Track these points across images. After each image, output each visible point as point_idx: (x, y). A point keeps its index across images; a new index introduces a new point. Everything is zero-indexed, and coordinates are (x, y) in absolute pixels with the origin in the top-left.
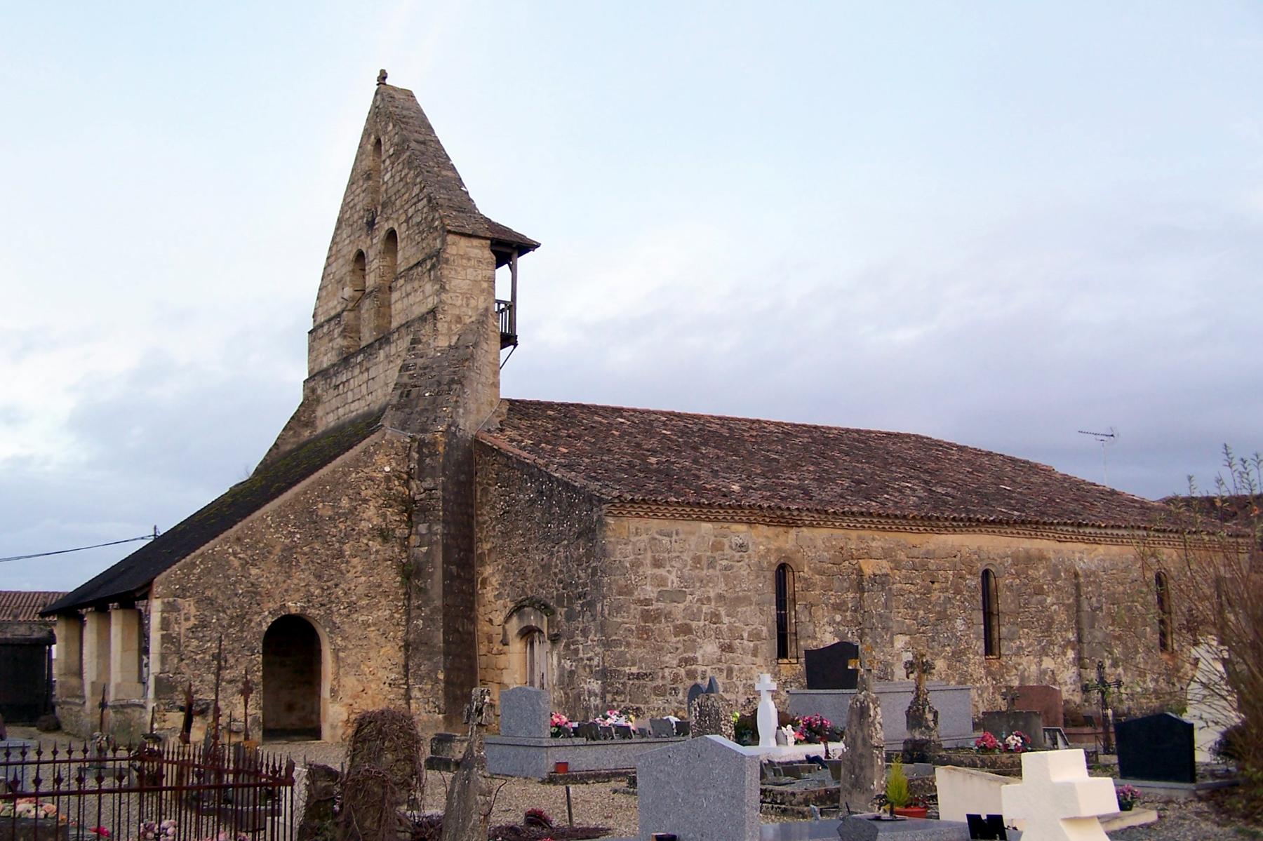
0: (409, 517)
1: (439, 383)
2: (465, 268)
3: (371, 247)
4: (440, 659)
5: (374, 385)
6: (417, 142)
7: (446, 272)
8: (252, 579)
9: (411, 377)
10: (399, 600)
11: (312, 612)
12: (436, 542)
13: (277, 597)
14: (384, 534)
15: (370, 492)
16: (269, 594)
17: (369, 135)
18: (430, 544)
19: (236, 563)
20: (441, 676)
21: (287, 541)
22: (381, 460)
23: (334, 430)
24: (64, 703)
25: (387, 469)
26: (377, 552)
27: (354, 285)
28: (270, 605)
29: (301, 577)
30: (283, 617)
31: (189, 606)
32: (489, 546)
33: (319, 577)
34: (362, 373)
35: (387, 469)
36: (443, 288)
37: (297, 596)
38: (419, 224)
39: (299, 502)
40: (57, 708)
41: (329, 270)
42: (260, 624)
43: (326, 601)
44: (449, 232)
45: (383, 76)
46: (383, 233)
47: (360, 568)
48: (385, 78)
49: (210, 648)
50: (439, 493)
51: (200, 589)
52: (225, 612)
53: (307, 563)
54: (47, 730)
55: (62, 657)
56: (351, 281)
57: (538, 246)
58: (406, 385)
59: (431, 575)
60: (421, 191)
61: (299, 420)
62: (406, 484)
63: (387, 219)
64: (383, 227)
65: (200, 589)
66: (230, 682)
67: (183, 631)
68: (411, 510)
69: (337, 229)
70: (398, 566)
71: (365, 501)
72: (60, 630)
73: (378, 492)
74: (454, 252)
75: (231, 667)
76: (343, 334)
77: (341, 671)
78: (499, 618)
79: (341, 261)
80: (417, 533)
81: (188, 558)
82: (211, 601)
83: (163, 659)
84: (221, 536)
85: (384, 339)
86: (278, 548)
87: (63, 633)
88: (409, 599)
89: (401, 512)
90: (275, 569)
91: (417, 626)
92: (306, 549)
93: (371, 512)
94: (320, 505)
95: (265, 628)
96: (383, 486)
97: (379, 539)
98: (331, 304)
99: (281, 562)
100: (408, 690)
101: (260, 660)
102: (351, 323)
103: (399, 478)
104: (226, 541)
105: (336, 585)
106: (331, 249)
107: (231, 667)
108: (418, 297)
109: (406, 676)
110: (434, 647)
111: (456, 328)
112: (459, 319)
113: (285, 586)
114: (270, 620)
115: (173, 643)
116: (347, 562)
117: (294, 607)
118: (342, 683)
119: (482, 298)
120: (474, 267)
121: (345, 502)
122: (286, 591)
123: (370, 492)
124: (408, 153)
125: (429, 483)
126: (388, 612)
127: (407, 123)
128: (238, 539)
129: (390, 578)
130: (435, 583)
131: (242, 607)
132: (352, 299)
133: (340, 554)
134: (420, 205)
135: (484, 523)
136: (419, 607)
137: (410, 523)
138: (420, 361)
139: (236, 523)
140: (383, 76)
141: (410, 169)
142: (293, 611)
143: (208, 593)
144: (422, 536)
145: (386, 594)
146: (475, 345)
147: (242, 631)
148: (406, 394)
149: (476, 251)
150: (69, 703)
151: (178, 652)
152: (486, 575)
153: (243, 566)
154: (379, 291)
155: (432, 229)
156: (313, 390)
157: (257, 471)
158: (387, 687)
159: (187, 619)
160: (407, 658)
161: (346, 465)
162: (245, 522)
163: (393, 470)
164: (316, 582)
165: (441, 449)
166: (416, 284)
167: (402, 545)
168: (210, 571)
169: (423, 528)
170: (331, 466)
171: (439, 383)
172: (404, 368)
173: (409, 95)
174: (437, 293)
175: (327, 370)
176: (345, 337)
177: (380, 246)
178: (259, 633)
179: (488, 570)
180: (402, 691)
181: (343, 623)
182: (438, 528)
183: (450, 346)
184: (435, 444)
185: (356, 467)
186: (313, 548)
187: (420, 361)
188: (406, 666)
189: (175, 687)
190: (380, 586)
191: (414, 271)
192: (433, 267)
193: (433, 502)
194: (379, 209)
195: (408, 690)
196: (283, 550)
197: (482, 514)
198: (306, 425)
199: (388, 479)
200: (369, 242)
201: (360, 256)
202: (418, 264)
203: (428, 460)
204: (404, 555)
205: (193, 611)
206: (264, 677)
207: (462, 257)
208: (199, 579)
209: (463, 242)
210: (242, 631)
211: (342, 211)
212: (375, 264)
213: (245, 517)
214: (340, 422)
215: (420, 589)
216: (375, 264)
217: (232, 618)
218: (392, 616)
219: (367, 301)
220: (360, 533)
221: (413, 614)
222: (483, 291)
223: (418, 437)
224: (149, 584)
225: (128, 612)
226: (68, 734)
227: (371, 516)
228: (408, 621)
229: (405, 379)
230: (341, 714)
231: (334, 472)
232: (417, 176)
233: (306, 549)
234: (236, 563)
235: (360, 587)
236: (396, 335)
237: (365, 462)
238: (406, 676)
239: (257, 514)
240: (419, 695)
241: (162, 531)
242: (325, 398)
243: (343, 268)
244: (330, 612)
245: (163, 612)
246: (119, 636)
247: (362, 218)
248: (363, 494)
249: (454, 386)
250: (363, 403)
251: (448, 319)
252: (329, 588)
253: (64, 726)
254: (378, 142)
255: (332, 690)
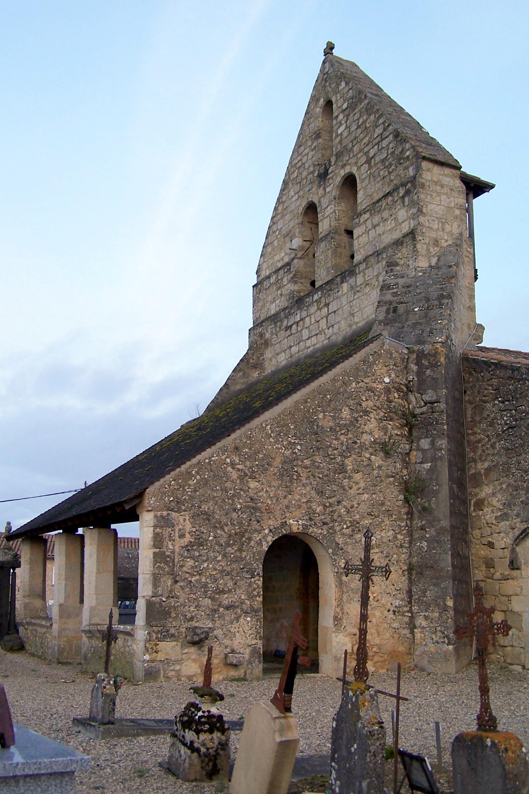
0: (410, 432)
1: (428, 300)
2: (439, 194)
3: (323, 196)
4: (448, 584)
5: (357, 306)
6: (370, 93)
7: (422, 196)
8: (251, 493)
9: (395, 294)
10: (401, 520)
11: (314, 531)
12: (441, 458)
13: (278, 513)
14: (386, 449)
15: (370, 403)
16: (269, 511)
17: (318, 100)
18: (434, 459)
19: (234, 475)
20: (450, 603)
21: (288, 453)
22: (381, 371)
23: (287, 368)
24: (29, 624)
25: (387, 380)
26: (380, 467)
27: (303, 236)
28: (271, 522)
29: (303, 492)
30: (285, 537)
31: (184, 521)
32: (486, 465)
33: (321, 493)
34: (319, 309)
35: (387, 380)
36: (420, 211)
37: (298, 513)
38: (383, 161)
39: (299, 410)
40: (21, 629)
41: (274, 228)
42: (260, 543)
43: (328, 520)
44: (424, 158)
45: (330, 47)
46: (338, 180)
47: (362, 485)
48: (332, 48)
49: (207, 568)
50: (443, 406)
51: (196, 502)
52: (222, 529)
53: (308, 478)
54: (11, 650)
55: (27, 579)
56: (300, 232)
57: (492, 187)
58: (391, 303)
59: (436, 493)
60: (385, 130)
61: (248, 362)
62: (405, 397)
63: (343, 166)
64: (338, 175)
65: (196, 502)
66: (227, 608)
67: (177, 549)
68: (412, 423)
69: (282, 190)
70: (400, 483)
71: (366, 413)
72: (25, 552)
73: (378, 404)
74: (429, 178)
75: (230, 591)
76: (294, 280)
77: (345, 598)
78: (503, 540)
79: (288, 217)
80: (418, 449)
81: (183, 468)
82: (208, 516)
83: (156, 580)
84: (219, 445)
85: (347, 272)
86: (279, 459)
87: (28, 556)
88: (411, 519)
89: (402, 426)
90: (276, 483)
91: (421, 548)
92: (307, 462)
93: (372, 425)
94: (321, 416)
95: (265, 548)
96: (383, 397)
97: (382, 454)
98: (277, 258)
99: (282, 475)
100: (412, 618)
101: (260, 583)
102: (292, 280)
103: (398, 390)
104: (224, 450)
105: (339, 502)
106: (276, 209)
107: (230, 591)
108: (391, 224)
109: (410, 602)
110: (442, 570)
111: (434, 250)
112: (436, 243)
113: (286, 502)
114: (270, 539)
115: (166, 563)
116: (350, 477)
117: (295, 525)
118: (346, 609)
119: (455, 225)
120: (446, 194)
121: (346, 413)
122: (287, 507)
123: (370, 403)
124: (366, 101)
125: (430, 396)
126: (391, 532)
127: (360, 82)
128: (237, 448)
129: (393, 496)
130: (441, 503)
131: (240, 524)
132: (301, 248)
133: (342, 469)
134: (384, 143)
135: (479, 441)
136: (422, 528)
137: (410, 438)
138: (401, 281)
139: (234, 431)
140: (330, 47)
141: (370, 115)
142: (295, 529)
143: (205, 507)
144: (424, 451)
145: (389, 514)
146: (457, 265)
147: (240, 550)
148: (392, 313)
149: (448, 179)
150: (34, 624)
151: (172, 573)
152: (483, 495)
153: (241, 478)
154: (336, 232)
155: (400, 159)
156: (261, 335)
157: (209, 409)
158: (391, 615)
159: (182, 536)
160: (411, 581)
161: (345, 373)
162: (243, 429)
163: (392, 381)
164: (318, 498)
165: (442, 359)
166: (386, 214)
167: (404, 461)
168: (206, 482)
169: (425, 443)
170: (331, 374)
171: (428, 300)
172: (385, 287)
173: (354, 65)
174: (414, 217)
175: (276, 315)
176: (296, 282)
177: (335, 193)
178: (259, 553)
179: (486, 491)
180: (406, 619)
181: (346, 544)
182: (443, 443)
183: (431, 266)
184: (435, 354)
185: (356, 377)
186: (314, 461)
187: (401, 281)
188: (410, 592)
189: (170, 613)
190: (383, 504)
191: (384, 203)
192: (408, 193)
193: (436, 415)
194: (333, 160)
195: (412, 618)
196: (284, 462)
197: (475, 433)
198: (255, 367)
199: (388, 391)
200: (321, 191)
201: (312, 209)
202: (389, 194)
203: (428, 372)
204: (405, 472)
205: (188, 526)
206: (264, 602)
207: (436, 183)
208: (195, 491)
209: (436, 169)
210: (240, 550)
211: (289, 172)
212: (329, 210)
213: (243, 425)
214: (294, 359)
215: (424, 509)
216: (329, 210)
217: (230, 536)
218: (395, 537)
219: (323, 245)
220: (362, 446)
221: (416, 536)
222: (456, 218)
223: (416, 348)
224: (140, 495)
225: (103, 531)
226: (33, 655)
227: (372, 429)
228: (410, 542)
229: (388, 297)
230: (344, 644)
231: (334, 380)
232: (378, 119)
233: (307, 462)
234: (234, 475)
235: (362, 505)
236: (363, 266)
237: (366, 372)
238: (410, 602)
239: (256, 422)
240: (424, 623)
241: (89, 483)
242: (274, 340)
243: (292, 222)
244: (332, 532)
245: (155, 527)
246: (95, 557)
247: (313, 172)
248: (364, 405)
249: (445, 301)
250: (321, 338)
251: (427, 241)
252: (331, 505)
253: (27, 647)
254: (329, 104)
255: (336, 618)
